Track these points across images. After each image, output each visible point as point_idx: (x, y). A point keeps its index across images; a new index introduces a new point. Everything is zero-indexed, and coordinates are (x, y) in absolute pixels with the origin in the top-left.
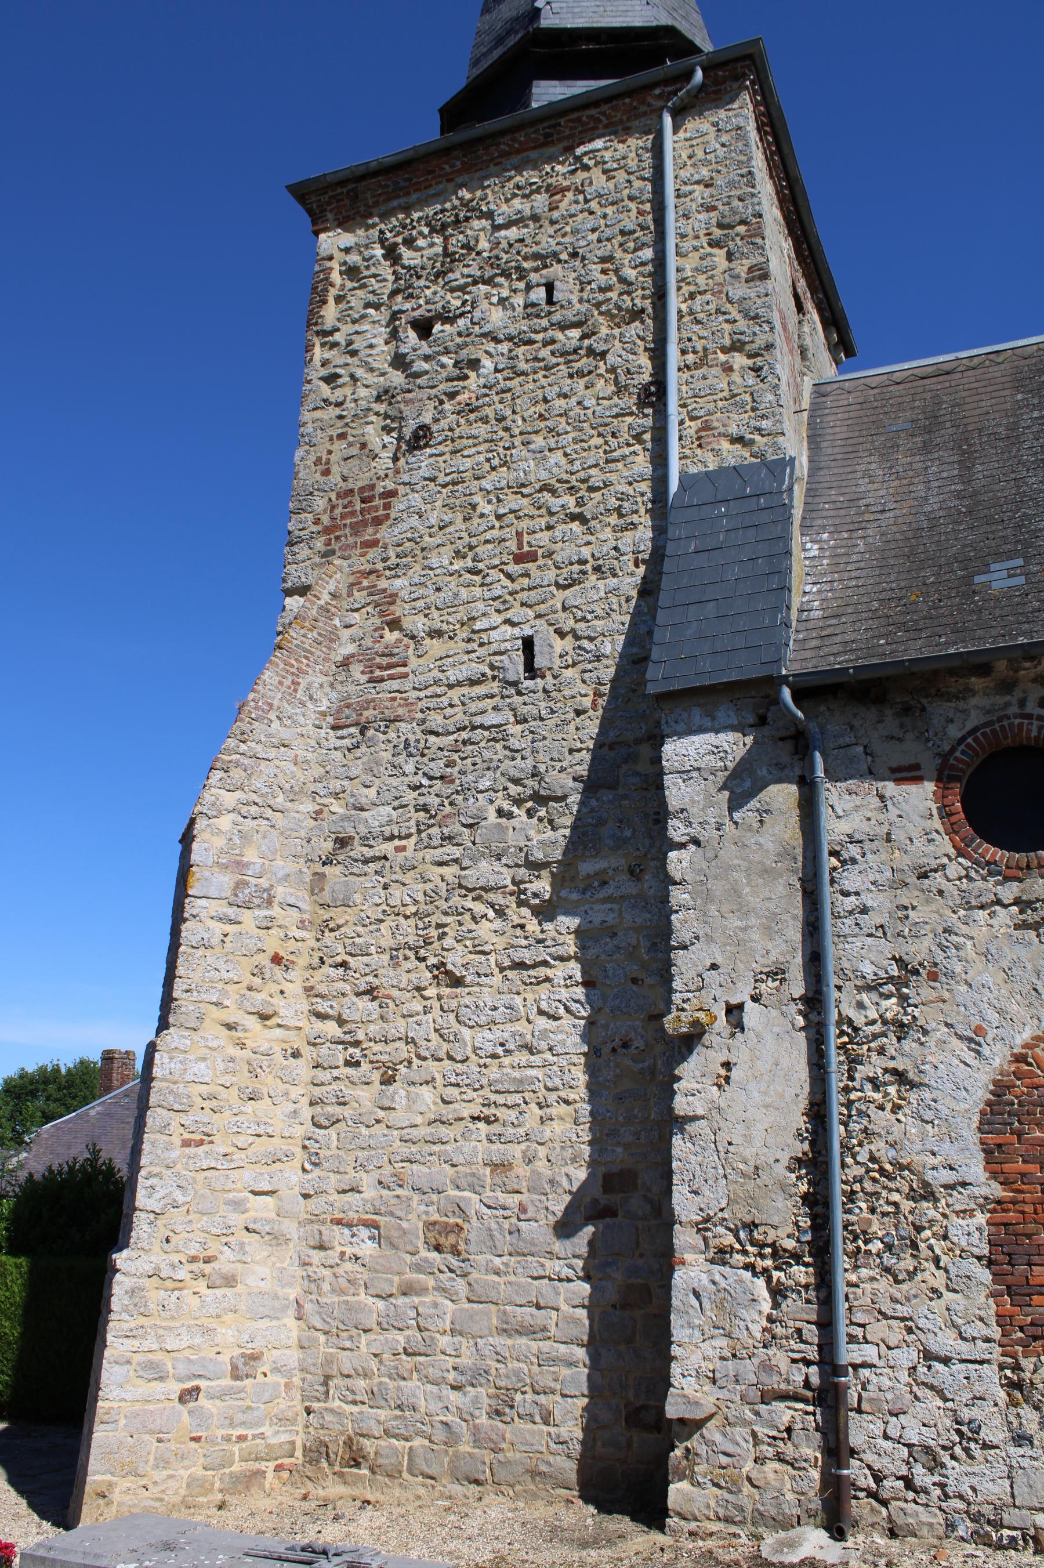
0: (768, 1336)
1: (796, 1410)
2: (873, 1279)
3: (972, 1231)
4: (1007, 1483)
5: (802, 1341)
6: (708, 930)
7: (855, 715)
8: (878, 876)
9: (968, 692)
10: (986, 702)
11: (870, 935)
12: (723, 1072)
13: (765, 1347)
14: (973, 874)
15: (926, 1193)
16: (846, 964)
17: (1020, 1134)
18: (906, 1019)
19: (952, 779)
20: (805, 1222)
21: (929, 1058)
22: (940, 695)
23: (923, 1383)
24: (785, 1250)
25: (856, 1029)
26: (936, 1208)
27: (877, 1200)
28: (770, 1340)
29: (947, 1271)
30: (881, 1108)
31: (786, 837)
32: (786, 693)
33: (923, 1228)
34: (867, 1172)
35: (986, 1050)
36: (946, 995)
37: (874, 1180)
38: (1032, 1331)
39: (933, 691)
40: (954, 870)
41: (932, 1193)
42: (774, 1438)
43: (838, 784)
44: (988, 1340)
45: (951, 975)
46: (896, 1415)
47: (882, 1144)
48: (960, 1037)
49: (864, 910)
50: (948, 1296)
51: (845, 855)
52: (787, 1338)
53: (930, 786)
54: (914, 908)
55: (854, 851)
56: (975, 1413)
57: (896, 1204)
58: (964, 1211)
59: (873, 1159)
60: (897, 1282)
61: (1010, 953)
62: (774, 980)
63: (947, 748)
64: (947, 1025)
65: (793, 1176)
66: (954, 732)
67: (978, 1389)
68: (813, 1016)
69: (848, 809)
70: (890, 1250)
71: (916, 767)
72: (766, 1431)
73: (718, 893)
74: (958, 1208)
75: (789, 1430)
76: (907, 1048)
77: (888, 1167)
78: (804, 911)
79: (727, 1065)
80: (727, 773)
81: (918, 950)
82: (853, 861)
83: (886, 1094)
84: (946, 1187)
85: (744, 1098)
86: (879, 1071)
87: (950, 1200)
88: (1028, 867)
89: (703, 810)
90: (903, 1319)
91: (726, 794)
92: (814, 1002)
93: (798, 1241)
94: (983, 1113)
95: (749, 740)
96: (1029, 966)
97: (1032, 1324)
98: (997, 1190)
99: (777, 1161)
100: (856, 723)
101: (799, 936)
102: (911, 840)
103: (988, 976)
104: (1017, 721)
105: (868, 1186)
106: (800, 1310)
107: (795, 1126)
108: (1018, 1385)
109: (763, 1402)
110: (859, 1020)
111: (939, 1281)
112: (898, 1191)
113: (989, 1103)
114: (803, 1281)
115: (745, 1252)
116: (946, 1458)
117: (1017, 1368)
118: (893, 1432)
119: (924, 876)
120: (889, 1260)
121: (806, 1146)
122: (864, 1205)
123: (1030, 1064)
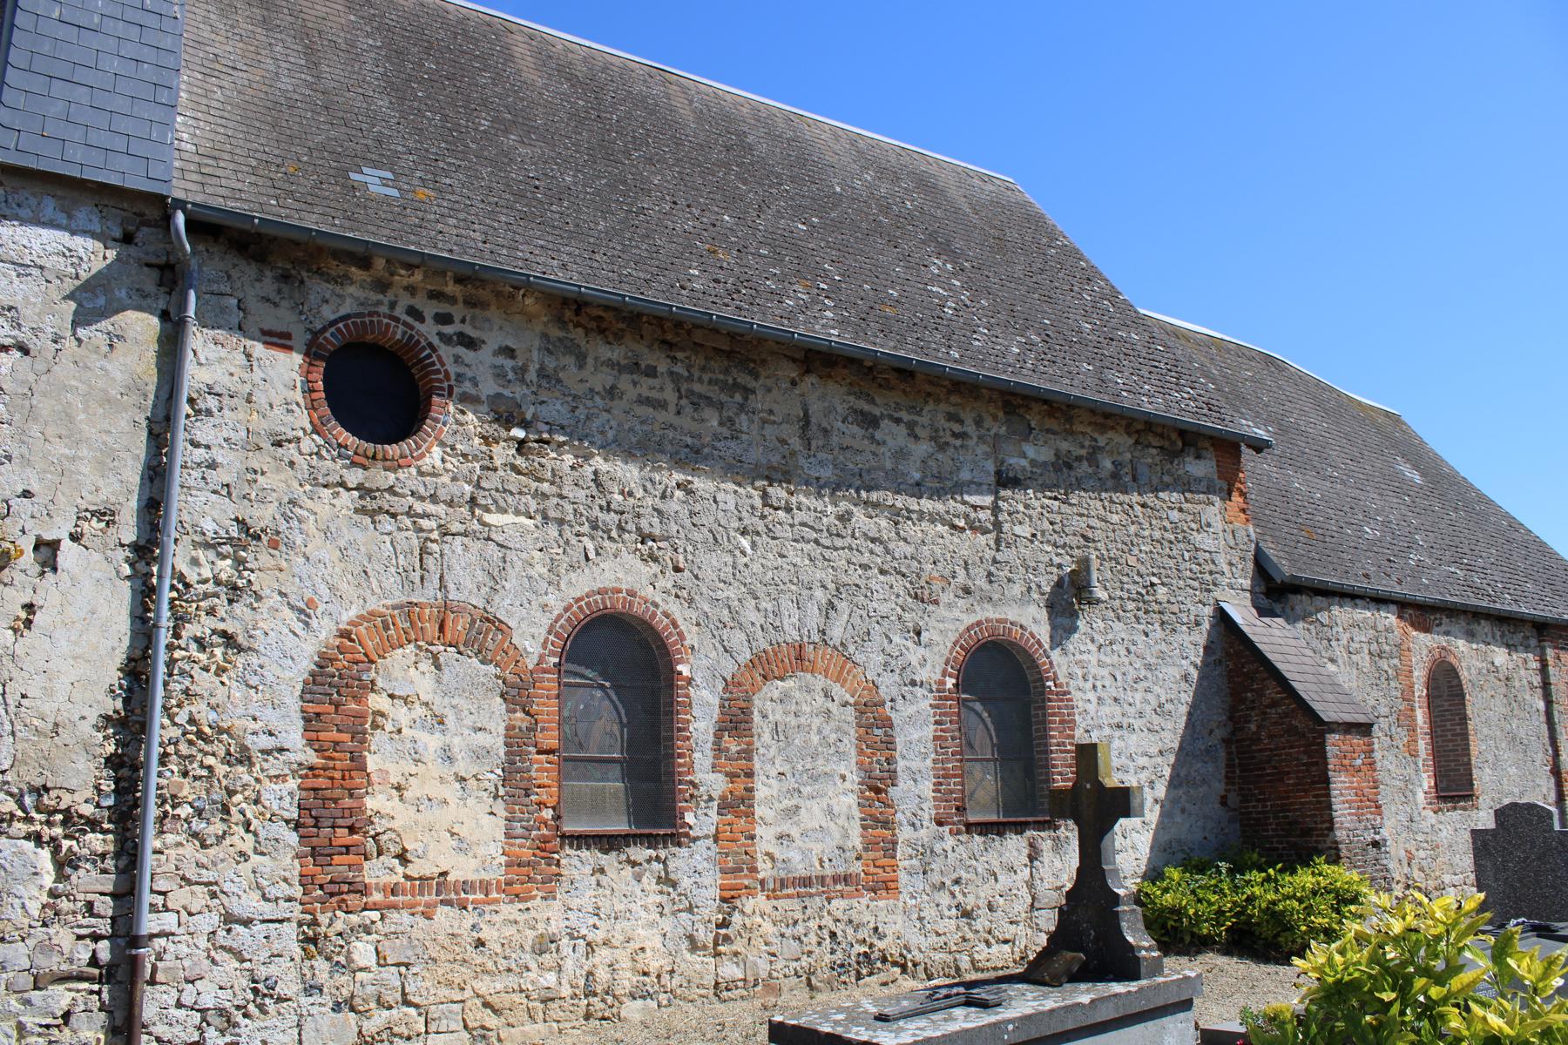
0: (50, 913)
1: (78, 991)
2: (179, 844)
3: (283, 796)
4: (296, 1031)
5: (92, 915)
6: (24, 450)
7: (235, 266)
8: (232, 434)
9: (344, 280)
10: (361, 294)
11: (215, 492)
12: (23, 615)
13: (45, 925)
14: (324, 453)
15: (245, 758)
16: (185, 517)
17: (337, 705)
18: (240, 583)
19: (318, 357)
20: (108, 786)
21: (261, 624)
22: (318, 272)
23: (222, 947)
24: (81, 816)
25: (187, 586)
26: (250, 772)
27: (191, 763)
28: (52, 914)
29: (256, 834)
30: (206, 669)
31: (139, 370)
32: (180, 219)
33: (235, 792)
34: (184, 734)
35: (314, 623)
36: (284, 564)
37: (191, 743)
38: (330, 888)
39: (314, 267)
40: (307, 445)
41: (249, 758)
42: (48, 1027)
43: (205, 330)
44: (289, 900)
45: (291, 546)
46: (192, 982)
47: (203, 707)
48: (292, 607)
49: (213, 465)
50: (255, 859)
51: (201, 405)
52: (74, 913)
53: (297, 358)
54: (263, 473)
55: (212, 402)
56: (273, 970)
57: (210, 768)
58: (277, 777)
59: (192, 721)
60: (204, 846)
61: (348, 534)
62: (100, 521)
63: (319, 327)
64: (281, 593)
65: (100, 735)
66: (328, 313)
67: (277, 947)
68: (141, 566)
69: (211, 358)
70: (200, 815)
71: (288, 336)
72: (37, 1020)
73: (45, 412)
74: (272, 772)
75: (67, 1016)
76: (238, 611)
77: (207, 730)
78: (147, 453)
79: (30, 607)
80: (78, 283)
81: (263, 516)
82: (209, 413)
83: (212, 655)
84: (263, 752)
85: (47, 646)
86: (208, 632)
87: (265, 766)
88: (374, 457)
89: (39, 315)
90: (207, 884)
91: (73, 305)
92: (146, 550)
93: (98, 806)
94: (305, 682)
95: (111, 254)
96: (363, 549)
97: (331, 882)
98: (312, 757)
99: (84, 718)
100: (235, 274)
101: (138, 479)
102: (271, 406)
103: (324, 551)
104: (386, 321)
105: (184, 748)
106: (93, 882)
107: (109, 681)
108: (314, 940)
109: (36, 988)
110: (192, 577)
111: (248, 844)
112: (213, 754)
113: (313, 674)
114: (100, 850)
115: (28, 820)
116: (239, 1018)
117: (315, 923)
118: (188, 999)
119: (279, 444)
120: (197, 825)
121: (119, 704)
122: (175, 769)
123: (352, 641)
